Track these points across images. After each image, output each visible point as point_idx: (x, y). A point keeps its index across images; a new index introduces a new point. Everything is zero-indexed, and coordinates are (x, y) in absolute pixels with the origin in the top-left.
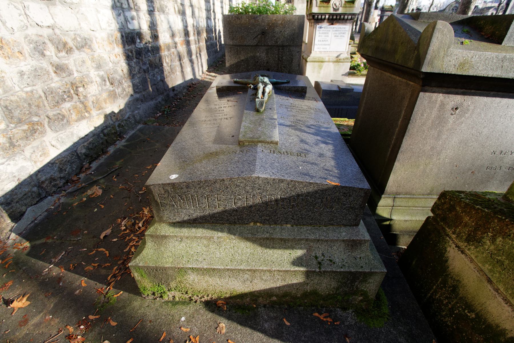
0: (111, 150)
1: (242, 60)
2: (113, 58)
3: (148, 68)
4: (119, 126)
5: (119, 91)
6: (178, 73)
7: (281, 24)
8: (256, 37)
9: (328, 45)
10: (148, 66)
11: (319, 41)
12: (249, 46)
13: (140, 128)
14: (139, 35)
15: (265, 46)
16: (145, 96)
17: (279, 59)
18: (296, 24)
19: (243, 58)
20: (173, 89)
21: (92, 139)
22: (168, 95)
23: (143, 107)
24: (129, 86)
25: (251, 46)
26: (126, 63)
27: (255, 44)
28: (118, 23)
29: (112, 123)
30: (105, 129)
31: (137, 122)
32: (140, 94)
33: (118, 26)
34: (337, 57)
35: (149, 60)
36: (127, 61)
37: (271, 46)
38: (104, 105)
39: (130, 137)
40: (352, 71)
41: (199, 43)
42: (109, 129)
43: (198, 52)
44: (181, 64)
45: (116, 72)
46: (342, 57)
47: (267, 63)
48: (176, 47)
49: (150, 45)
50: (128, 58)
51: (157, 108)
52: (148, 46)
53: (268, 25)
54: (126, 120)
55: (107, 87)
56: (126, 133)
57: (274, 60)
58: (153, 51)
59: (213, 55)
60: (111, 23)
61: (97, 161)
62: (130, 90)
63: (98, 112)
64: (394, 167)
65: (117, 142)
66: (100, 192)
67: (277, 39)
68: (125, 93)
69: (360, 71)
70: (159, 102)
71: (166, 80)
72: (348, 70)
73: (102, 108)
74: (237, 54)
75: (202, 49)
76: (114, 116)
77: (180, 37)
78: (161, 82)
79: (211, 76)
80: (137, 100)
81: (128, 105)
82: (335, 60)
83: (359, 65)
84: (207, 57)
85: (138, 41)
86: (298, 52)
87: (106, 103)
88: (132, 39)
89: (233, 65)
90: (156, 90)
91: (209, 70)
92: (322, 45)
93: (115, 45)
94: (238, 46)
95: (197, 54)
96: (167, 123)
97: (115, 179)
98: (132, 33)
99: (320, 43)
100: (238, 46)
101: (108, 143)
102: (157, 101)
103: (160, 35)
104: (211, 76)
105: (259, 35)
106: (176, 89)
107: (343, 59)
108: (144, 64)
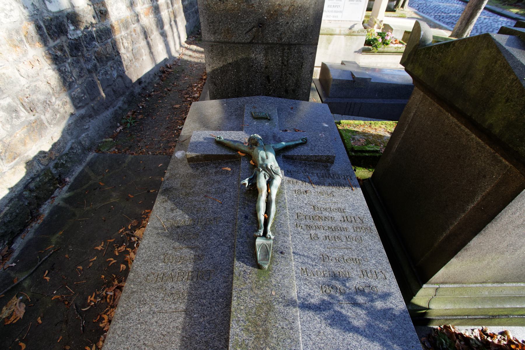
0: (46, 209)
1: (230, 64)
2: (25, 68)
3: (95, 66)
4: (56, 166)
5: (46, 117)
6: (144, 57)
7: (289, 11)
8: (250, 30)
9: (340, 12)
10: (96, 61)
11: (328, 6)
12: (239, 43)
13: (92, 159)
14: (73, 17)
15: (263, 43)
16: (96, 107)
17: (283, 63)
18: (311, 12)
19: (230, 61)
20: (139, 81)
21: (8, 208)
22: (132, 94)
23: (93, 126)
24: (65, 104)
25: (243, 43)
26: (54, 70)
27: (249, 41)
28: (26, 7)
29: (42, 167)
30: (30, 183)
31: (87, 150)
32: (86, 108)
33: (26, 12)
34: (350, 29)
35: (95, 52)
36: (54, 66)
37: (272, 43)
38: (21, 148)
39: (76, 179)
40: (366, 47)
41: (173, 6)
42: (38, 179)
43: (173, 19)
44: (148, 43)
45: (36, 89)
46: (356, 28)
47: (266, 68)
48: (138, 21)
49: (94, 29)
50: (56, 60)
51: (117, 118)
52: (91, 31)
53: (268, 12)
54: (67, 154)
55: (23, 119)
56: (68, 172)
57: (276, 65)
58: (100, 37)
59: (194, 17)
60: (11, 10)
61: (22, 236)
62: (69, 108)
63: (12, 163)
64: (449, 262)
65: (56, 192)
66: (20, 311)
67: (281, 34)
68: (58, 116)
69: (376, 47)
70: (120, 108)
71: (126, 73)
72: (362, 46)
73: (19, 155)
74: (222, 55)
75: (177, 13)
76: (45, 157)
77: (144, 3)
78: (120, 79)
79: (191, 50)
80: (82, 117)
81: (68, 131)
82: (347, 32)
83: (375, 39)
84: (185, 23)
85: (72, 28)
86: (311, 54)
87: (25, 144)
88: (60, 27)
89: (217, 70)
90: (112, 93)
91: (188, 42)
92: (332, 11)
93: (27, 45)
94: (222, 43)
95: (171, 21)
96: (130, 147)
97: (48, 278)
98: (57, 18)
99: (330, 9)
100: (222, 43)
101: (40, 201)
102: (116, 108)
103: (109, 9)
104: (191, 50)
105: (253, 27)
106: (143, 80)
107: (358, 32)
108: (88, 60)
